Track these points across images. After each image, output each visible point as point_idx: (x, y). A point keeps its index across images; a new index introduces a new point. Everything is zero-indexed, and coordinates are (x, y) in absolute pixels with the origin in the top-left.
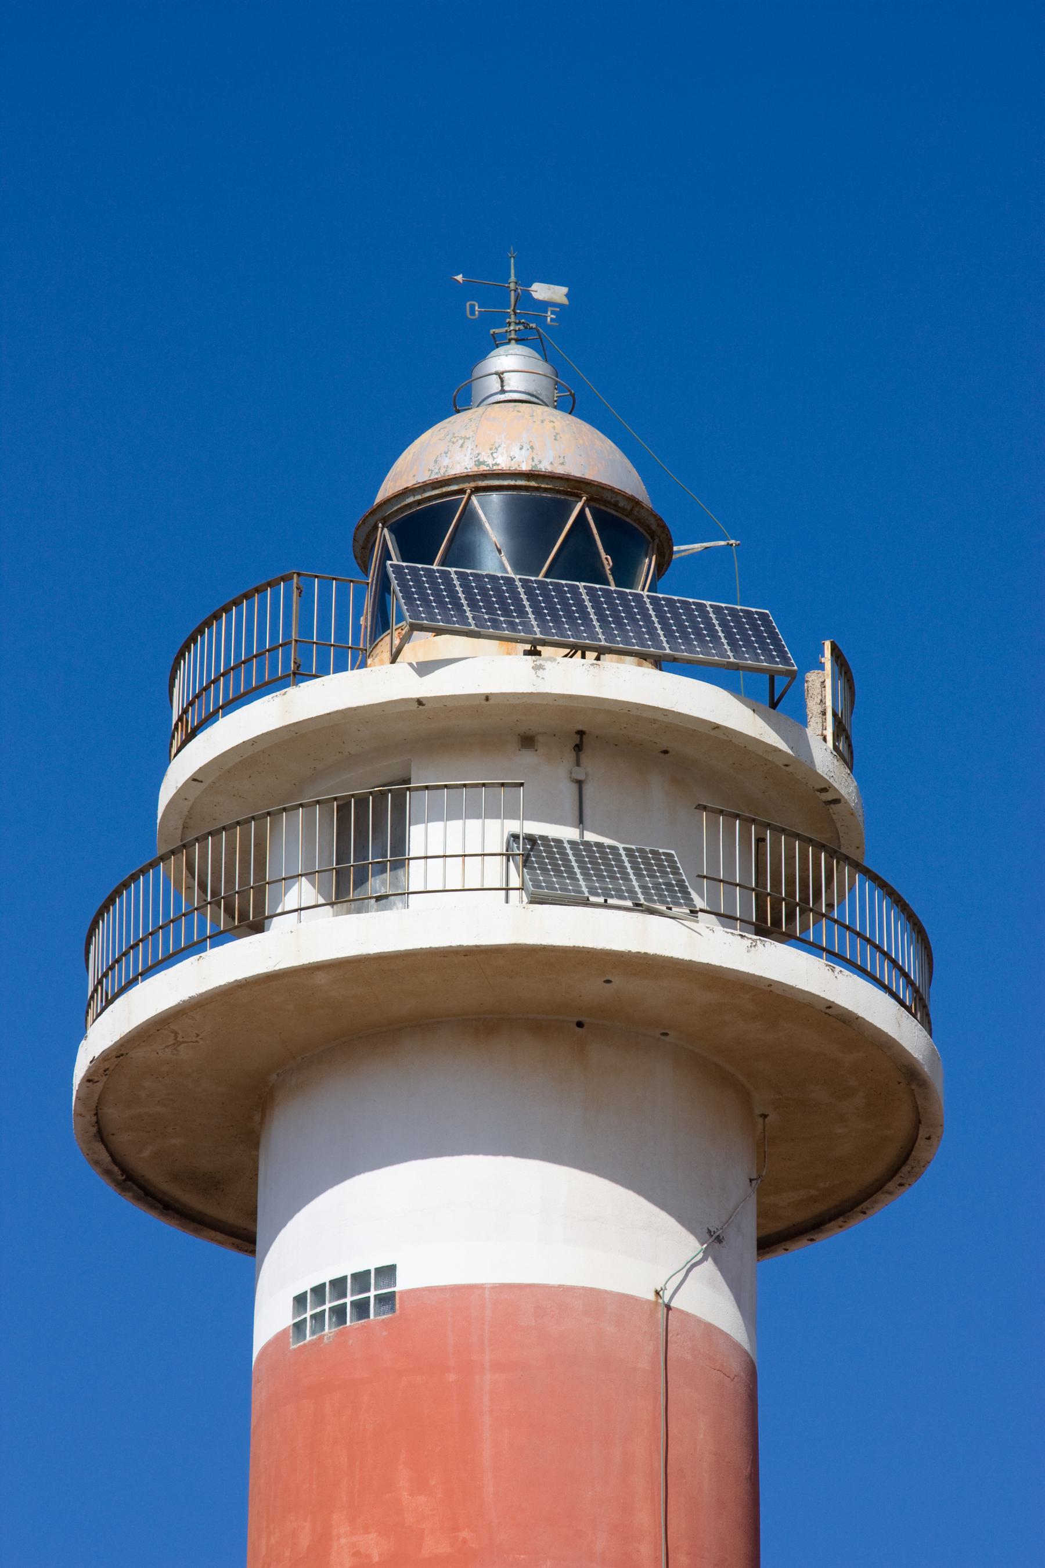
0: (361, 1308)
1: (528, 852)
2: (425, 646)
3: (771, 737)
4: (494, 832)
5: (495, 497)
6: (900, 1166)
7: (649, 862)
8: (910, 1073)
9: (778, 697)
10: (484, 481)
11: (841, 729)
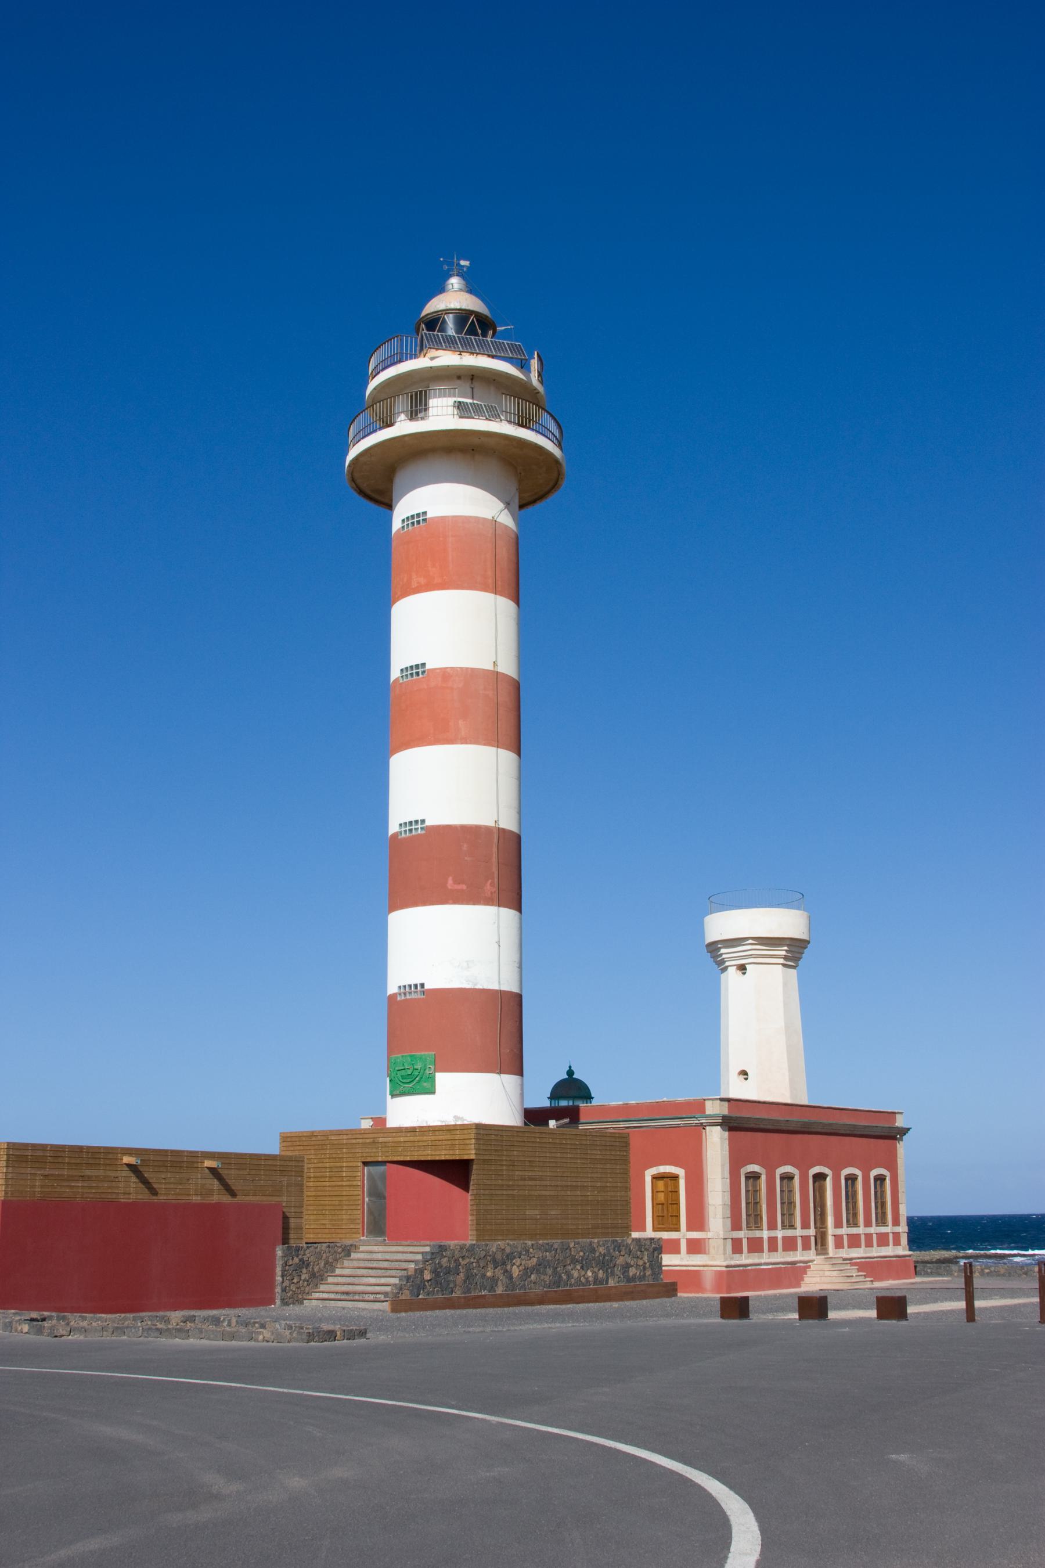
0: (418, 522)
1: (459, 406)
2: (433, 353)
3: (521, 376)
4: (450, 401)
5: (451, 316)
6: (555, 486)
7: (490, 408)
8: (556, 461)
9: (523, 365)
10: (447, 311)
11: (539, 375)
